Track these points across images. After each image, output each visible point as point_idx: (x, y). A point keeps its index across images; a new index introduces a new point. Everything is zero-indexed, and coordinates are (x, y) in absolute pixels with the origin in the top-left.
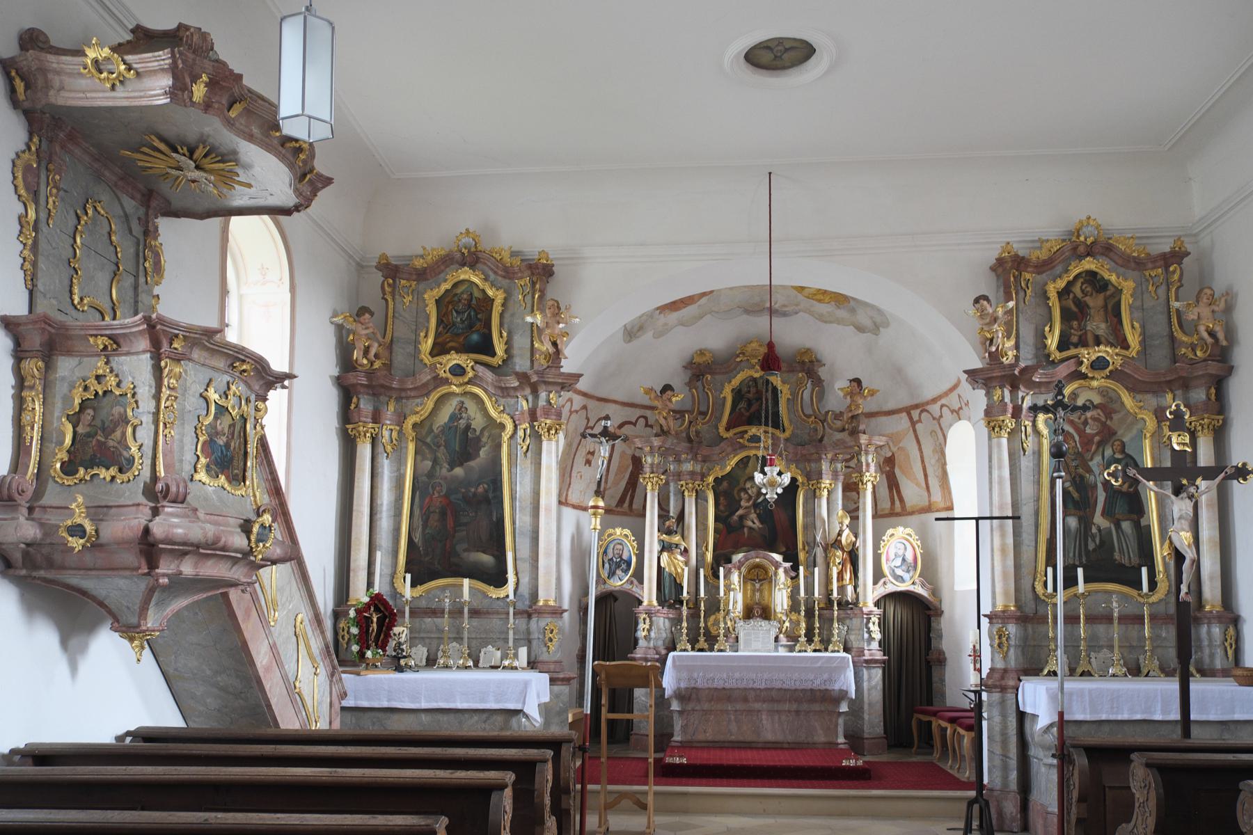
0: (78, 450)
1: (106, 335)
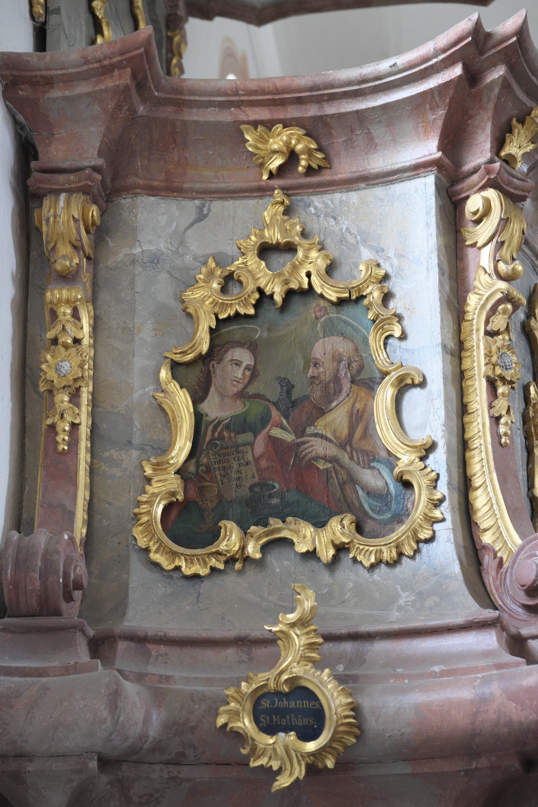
0: (208, 471)
1: (298, 123)
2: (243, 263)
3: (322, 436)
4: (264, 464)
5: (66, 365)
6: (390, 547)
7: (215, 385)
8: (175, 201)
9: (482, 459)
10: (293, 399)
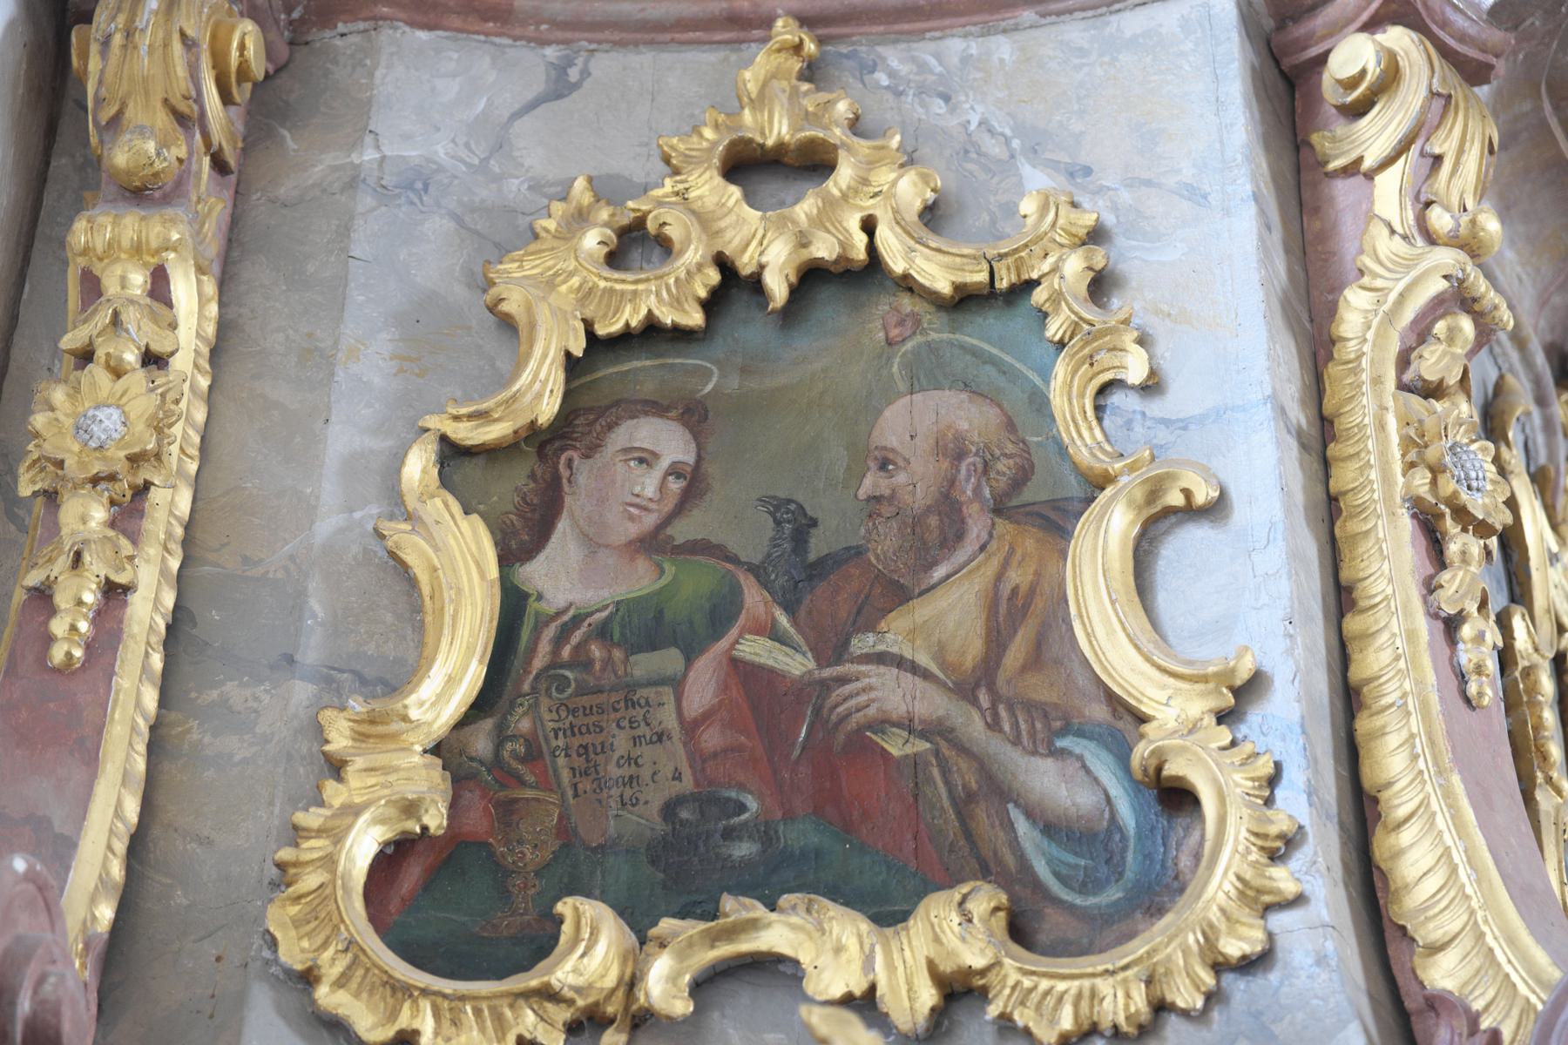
0: (533, 755)
2: (677, 194)
3: (900, 662)
4: (712, 738)
5: (109, 417)
6: (1125, 981)
7: (572, 516)
8: (487, 46)
9: (1412, 736)
10: (812, 556)
